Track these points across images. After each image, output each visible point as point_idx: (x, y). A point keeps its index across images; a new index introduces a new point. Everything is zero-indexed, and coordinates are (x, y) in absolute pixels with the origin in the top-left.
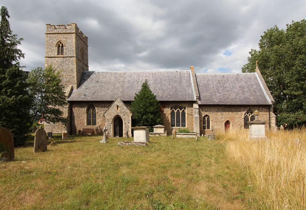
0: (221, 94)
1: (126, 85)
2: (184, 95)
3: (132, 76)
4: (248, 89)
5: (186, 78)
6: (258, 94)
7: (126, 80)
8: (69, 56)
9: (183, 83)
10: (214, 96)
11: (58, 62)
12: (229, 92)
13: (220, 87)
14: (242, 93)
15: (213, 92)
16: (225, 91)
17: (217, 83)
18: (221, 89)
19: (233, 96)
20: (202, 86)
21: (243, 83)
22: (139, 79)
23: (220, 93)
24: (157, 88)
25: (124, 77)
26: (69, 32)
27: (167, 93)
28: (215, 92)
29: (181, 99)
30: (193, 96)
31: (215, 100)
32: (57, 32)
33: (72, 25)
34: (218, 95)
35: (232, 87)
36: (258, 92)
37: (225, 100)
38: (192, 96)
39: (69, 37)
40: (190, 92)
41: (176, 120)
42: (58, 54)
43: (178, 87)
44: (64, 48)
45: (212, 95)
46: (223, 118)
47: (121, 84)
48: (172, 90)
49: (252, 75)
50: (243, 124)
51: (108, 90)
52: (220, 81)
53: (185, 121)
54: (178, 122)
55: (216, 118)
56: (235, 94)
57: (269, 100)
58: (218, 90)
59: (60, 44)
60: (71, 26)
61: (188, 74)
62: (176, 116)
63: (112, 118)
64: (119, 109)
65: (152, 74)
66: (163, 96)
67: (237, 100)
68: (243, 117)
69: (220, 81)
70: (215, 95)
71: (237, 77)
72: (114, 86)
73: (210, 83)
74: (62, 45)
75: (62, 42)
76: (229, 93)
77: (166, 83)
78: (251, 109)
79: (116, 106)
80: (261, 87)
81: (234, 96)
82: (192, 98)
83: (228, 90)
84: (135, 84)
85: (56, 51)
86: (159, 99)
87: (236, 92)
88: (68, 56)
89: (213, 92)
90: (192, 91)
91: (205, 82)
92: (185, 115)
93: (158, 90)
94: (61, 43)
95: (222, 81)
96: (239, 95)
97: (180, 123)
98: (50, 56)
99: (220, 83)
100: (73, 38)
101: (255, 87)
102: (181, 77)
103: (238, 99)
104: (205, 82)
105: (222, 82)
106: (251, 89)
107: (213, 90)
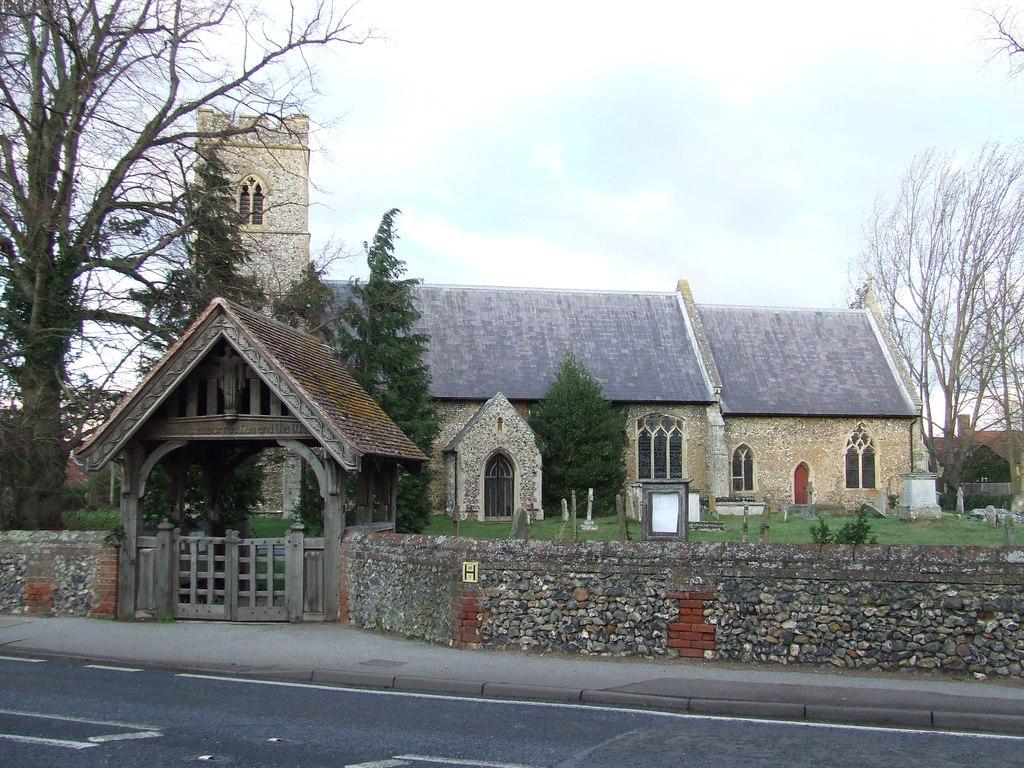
1: (482, 343)
3: (493, 305)
4: (853, 363)
6: (879, 382)
8: (284, 229)
14: (835, 376)
21: (835, 345)
22: (520, 319)
23: (775, 376)
24: (588, 355)
28: (760, 371)
30: (704, 385)
35: (809, 356)
36: (879, 373)
40: (692, 372)
50: (845, 473)
54: (660, 469)
56: (817, 381)
64: (505, 429)
65: (559, 302)
67: (826, 400)
68: (845, 451)
70: (764, 383)
74: (258, 188)
75: (258, 180)
78: (864, 426)
80: (885, 360)
83: (797, 365)
86: (610, 397)
87: (820, 372)
88: (279, 230)
90: (698, 370)
91: (728, 336)
92: (680, 446)
94: (252, 181)
95: (775, 333)
96: (828, 382)
99: (770, 341)
101: (869, 356)
102: (652, 316)
106: (859, 363)
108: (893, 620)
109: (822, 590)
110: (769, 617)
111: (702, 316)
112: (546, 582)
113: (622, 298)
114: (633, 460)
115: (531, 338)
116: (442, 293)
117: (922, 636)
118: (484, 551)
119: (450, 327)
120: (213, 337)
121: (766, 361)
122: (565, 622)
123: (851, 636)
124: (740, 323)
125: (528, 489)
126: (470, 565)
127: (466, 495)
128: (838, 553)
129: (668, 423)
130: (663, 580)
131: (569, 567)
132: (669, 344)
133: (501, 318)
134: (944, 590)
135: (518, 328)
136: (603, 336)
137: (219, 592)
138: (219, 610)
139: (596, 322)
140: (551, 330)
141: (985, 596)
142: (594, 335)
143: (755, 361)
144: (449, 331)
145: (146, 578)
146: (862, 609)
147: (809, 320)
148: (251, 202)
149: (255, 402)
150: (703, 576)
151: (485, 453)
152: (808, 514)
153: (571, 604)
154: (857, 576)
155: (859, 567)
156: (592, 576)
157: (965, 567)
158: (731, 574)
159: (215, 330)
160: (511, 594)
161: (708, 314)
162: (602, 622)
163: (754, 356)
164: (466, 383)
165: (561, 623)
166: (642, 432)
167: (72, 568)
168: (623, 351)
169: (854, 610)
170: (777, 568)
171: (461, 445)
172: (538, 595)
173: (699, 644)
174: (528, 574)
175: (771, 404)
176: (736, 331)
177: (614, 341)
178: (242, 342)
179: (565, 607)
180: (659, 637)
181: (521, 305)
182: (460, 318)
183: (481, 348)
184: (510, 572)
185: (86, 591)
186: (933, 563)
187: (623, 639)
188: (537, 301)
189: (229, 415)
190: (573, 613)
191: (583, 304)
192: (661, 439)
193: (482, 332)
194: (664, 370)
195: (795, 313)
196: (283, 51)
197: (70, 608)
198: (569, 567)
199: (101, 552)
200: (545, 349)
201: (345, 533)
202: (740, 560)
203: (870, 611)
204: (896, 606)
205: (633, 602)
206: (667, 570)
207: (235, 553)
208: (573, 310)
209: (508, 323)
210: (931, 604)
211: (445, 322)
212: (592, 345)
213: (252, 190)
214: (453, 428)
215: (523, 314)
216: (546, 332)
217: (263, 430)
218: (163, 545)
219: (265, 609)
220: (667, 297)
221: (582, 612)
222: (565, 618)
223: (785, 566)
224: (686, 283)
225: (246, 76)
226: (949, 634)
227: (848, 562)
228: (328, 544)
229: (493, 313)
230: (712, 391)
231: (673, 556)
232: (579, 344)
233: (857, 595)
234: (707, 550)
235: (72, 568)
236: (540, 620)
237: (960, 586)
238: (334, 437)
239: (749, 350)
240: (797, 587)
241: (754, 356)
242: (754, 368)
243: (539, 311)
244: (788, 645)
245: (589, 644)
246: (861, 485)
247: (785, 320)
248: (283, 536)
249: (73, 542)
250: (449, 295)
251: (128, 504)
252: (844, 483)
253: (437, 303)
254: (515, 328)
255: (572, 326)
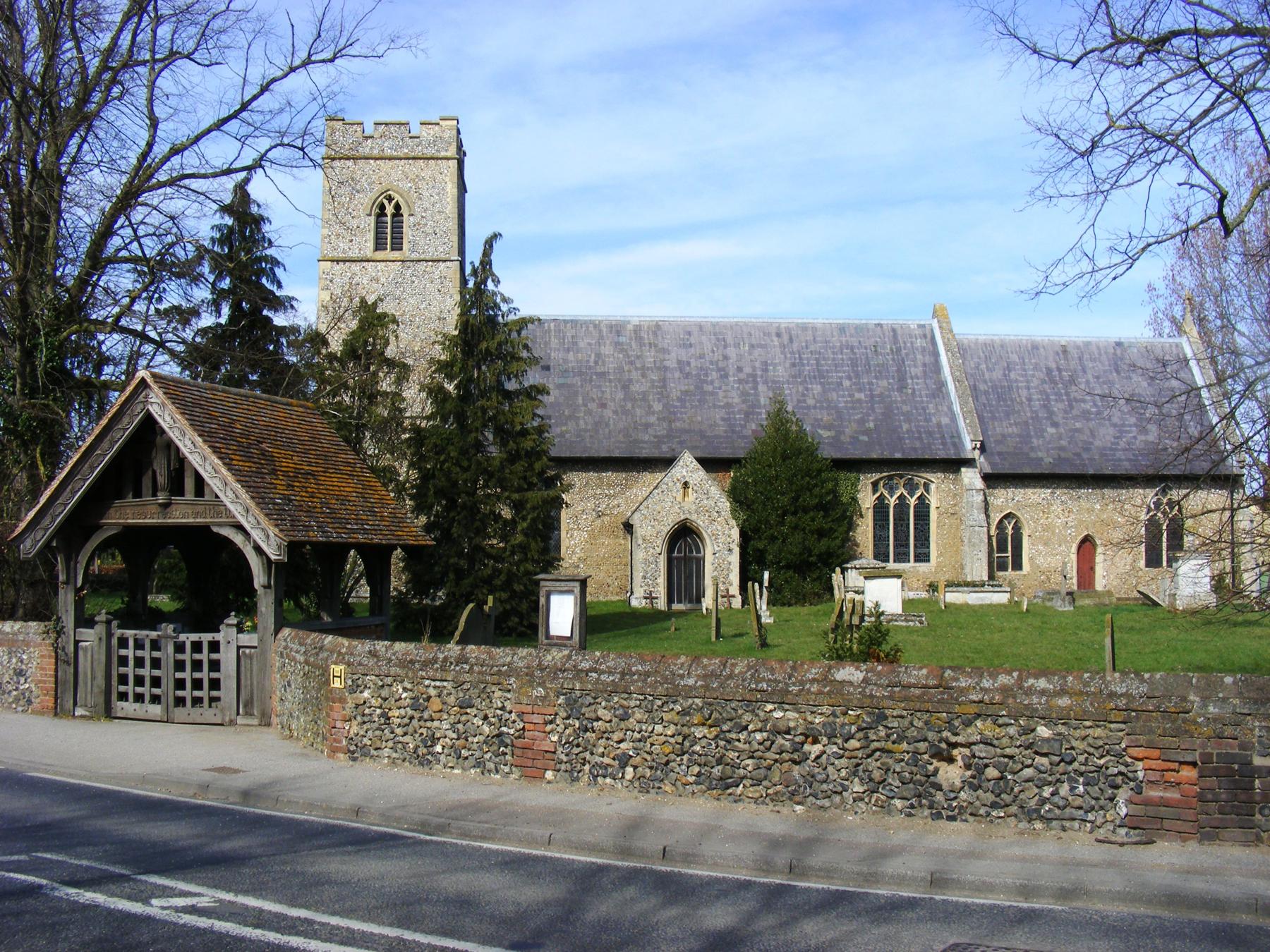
0: (1062, 430)
2: (923, 435)
3: (693, 340)
5: (919, 357)
7: (671, 363)
8: (428, 256)
9: (912, 378)
10: (1038, 438)
11: (377, 281)
12: (1091, 420)
13: (1056, 400)
14: (1135, 425)
15: (1032, 418)
16: (1076, 418)
17: (1044, 382)
18: (1061, 406)
19: (1106, 435)
20: (986, 393)
22: (726, 358)
23: (1055, 425)
24: (811, 402)
25: (656, 346)
26: (431, 152)
27: (854, 426)
28: (1036, 418)
29: (915, 449)
30: (959, 437)
31: (1040, 454)
32: (375, 152)
33: (441, 122)
34: (1052, 435)
37: (1078, 455)
38: (957, 440)
39: (426, 174)
40: (945, 421)
41: (895, 537)
42: (379, 245)
43: (896, 396)
44: (407, 220)
45: (1029, 436)
46: (1070, 524)
47: (653, 381)
48: (872, 408)
49: (1171, 346)
51: (603, 406)
52: (1056, 373)
53: (927, 539)
54: (902, 543)
55: (1046, 528)
56: (1111, 431)
57: (1236, 333)
58: (1051, 414)
59: (386, 202)
60: (437, 128)
61: (925, 336)
62: (895, 520)
63: (664, 534)
64: (692, 496)
65: (778, 335)
66: (842, 438)
67: (1119, 455)
69: (1056, 373)
70: (1041, 433)
71: (1115, 354)
72: (625, 388)
73: (1017, 381)
74: (398, 207)
75: (397, 197)
76: (1092, 424)
77: (841, 378)
79: (679, 486)
81: (1108, 438)
82: (954, 445)
84: (712, 382)
85: (371, 236)
86: (827, 452)
87: (1115, 420)
88: (422, 257)
89: (1032, 418)
91: (997, 374)
93: (815, 407)
94: (390, 199)
95: (1059, 370)
97: (908, 546)
98: (341, 256)
100: (447, 179)
102: (899, 350)
103: (1125, 450)
104: (997, 374)
105: (1061, 377)
107: (1032, 412)
108: (722, 743)
109: (655, 707)
110: (606, 735)
111: (961, 351)
112: (405, 689)
113: (860, 329)
114: (865, 532)
115: (740, 381)
116: (630, 327)
117: (749, 762)
118: (352, 654)
119: (636, 369)
120: (139, 413)
121: (1045, 406)
122: (422, 734)
123: (682, 760)
124: (1015, 358)
125: (721, 568)
126: (337, 669)
127: (644, 577)
128: (675, 665)
129: (911, 488)
130: (509, 691)
131: (424, 674)
132: (917, 385)
133: (702, 356)
134: (771, 711)
135: (723, 369)
136: (832, 377)
137: (156, 691)
138: (156, 710)
139: (824, 359)
140: (766, 370)
141: (810, 718)
142: (820, 376)
143: (1030, 406)
144: (635, 375)
145: (85, 673)
146: (692, 729)
147: (1106, 353)
148: (389, 225)
149: (189, 484)
150: (545, 688)
151: (667, 525)
152: (1060, 603)
153: (426, 715)
154: (689, 693)
155: (691, 682)
156: (445, 684)
157: (794, 684)
158: (570, 686)
159: (141, 406)
160: (373, 702)
161: (972, 345)
162: (454, 736)
163: (1029, 400)
164: (652, 439)
165: (417, 735)
166: (877, 498)
167: (14, 660)
168: (857, 395)
169: (685, 730)
170: (613, 681)
171: (636, 516)
172: (398, 703)
173: (539, 764)
174: (389, 680)
175: (1046, 461)
176: (1009, 368)
177: (847, 383)
178: (168, 418)
179: (421, 717)
180: (505, 754)
181: (730, 340)
182: (650, 357)
183: (675, 394)
184: (373, 677)
185: (27, 686)
186: (763, 680)
187: (472, 755)
188: (750, 334)
189: (162, 498)
190: (429, 724)
191: (810, 338)
192: (902, 505)
193: (677, 375)
194: (908, 421)
195: (1087, 344)
196: (286, 76)
197: (13, 702)
198: (424, 674)
199: (40, 645)
200: (757, 395)
201: (277, 632)
202: (581, 671)
203: (699, 732)
204: (725, 728)
205: (481, 715)
206: (513, 679)
207: (171, 649)
208: (795, 346)
209: (711, 363)
210: (760, 725)
211: (631, 363)
212: (817, 389)
213: (390, 210)
214: (636, 495)
215: (731, 352)
216: (759, 373)
217: (197, 515)
218: (100, 639)
219: (201, 710)
220: (920, 326)
221: (436, 723)
222: (422, 730)
223: (622, 679)
224: (943, 309)
225: (244, 107)
226: (776, 761)
227: (682, 677)
228: (261, 640)
229: (692, 350)
230: (968, 445)
231: (520, 664)
232: (801, 389)
233: (688, 714)
234: (553, 658)
235: (14, 660)
236: (399, 731)
237: (787, 707)
238: (258, 523)
239: (1024, 393)
240: (632, 703)
241: (1029, 400)
242: (1029, 414)
243: (752, 346)
244: (623, 766)
245: (442, 758)
246: (1010, 570)
247: (1074, 353)
248: (218, 631)
249: (15, 634)
250: (638, 329)
251: (66, 593)
252: (1142, 563)
253: (622, 339)
254: (719, 370)
255: (793, 365)
